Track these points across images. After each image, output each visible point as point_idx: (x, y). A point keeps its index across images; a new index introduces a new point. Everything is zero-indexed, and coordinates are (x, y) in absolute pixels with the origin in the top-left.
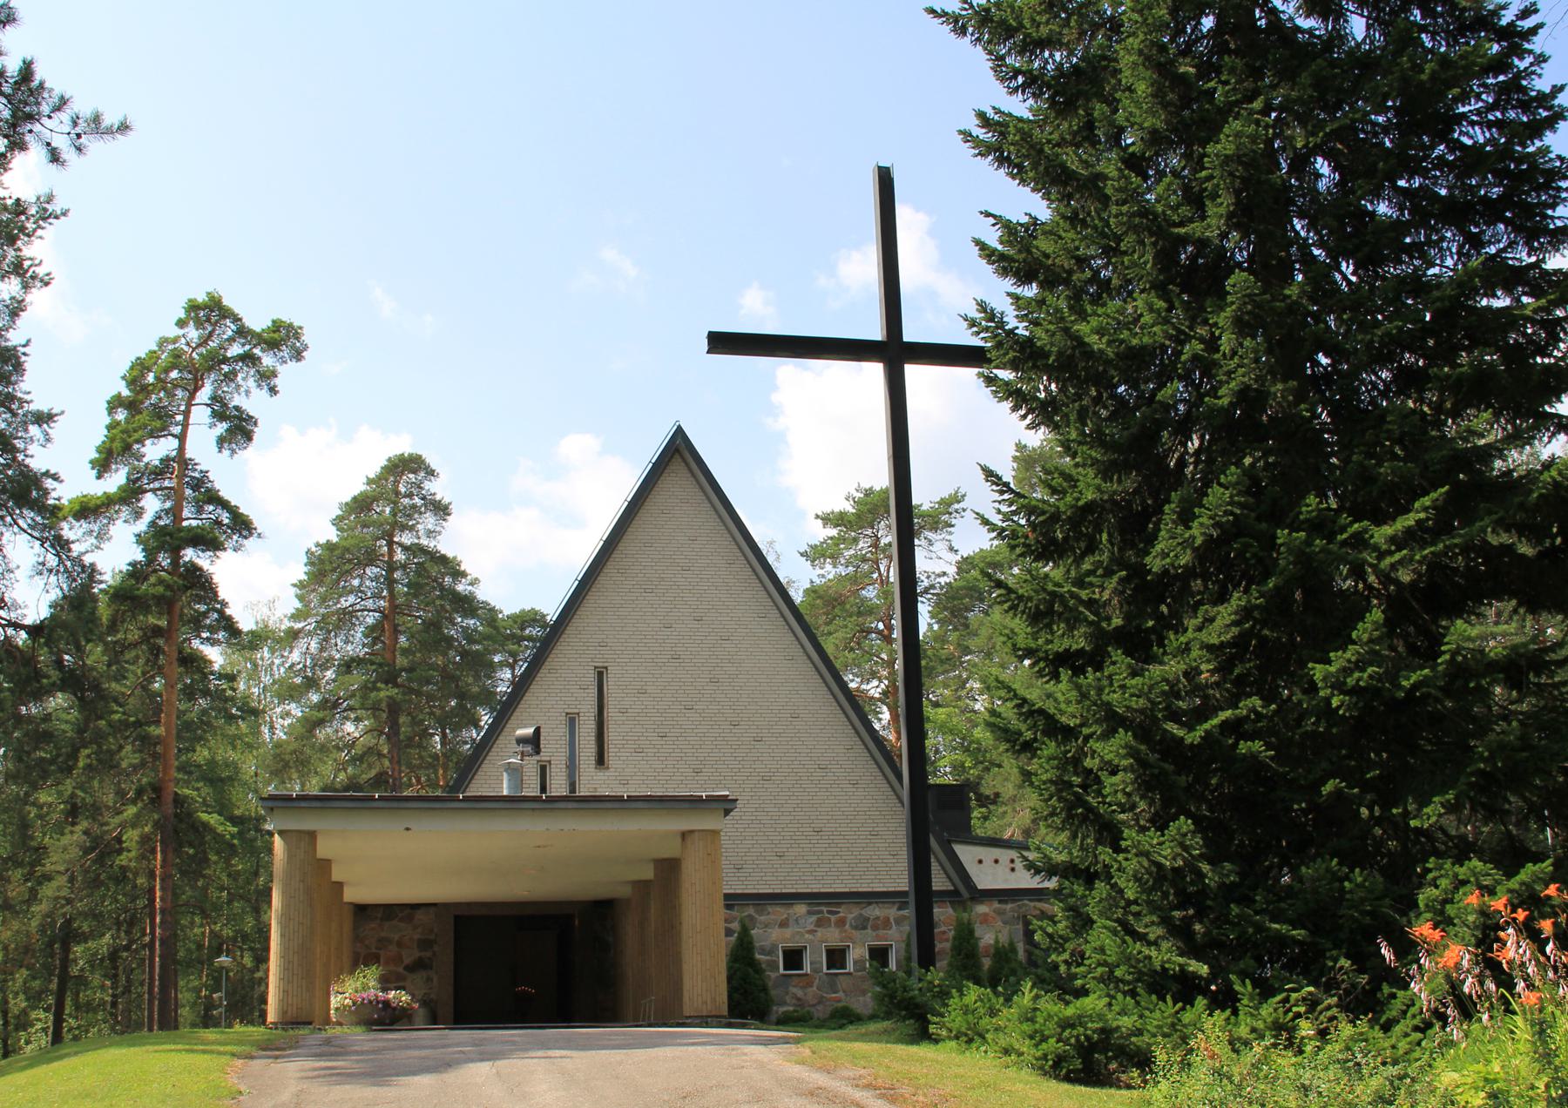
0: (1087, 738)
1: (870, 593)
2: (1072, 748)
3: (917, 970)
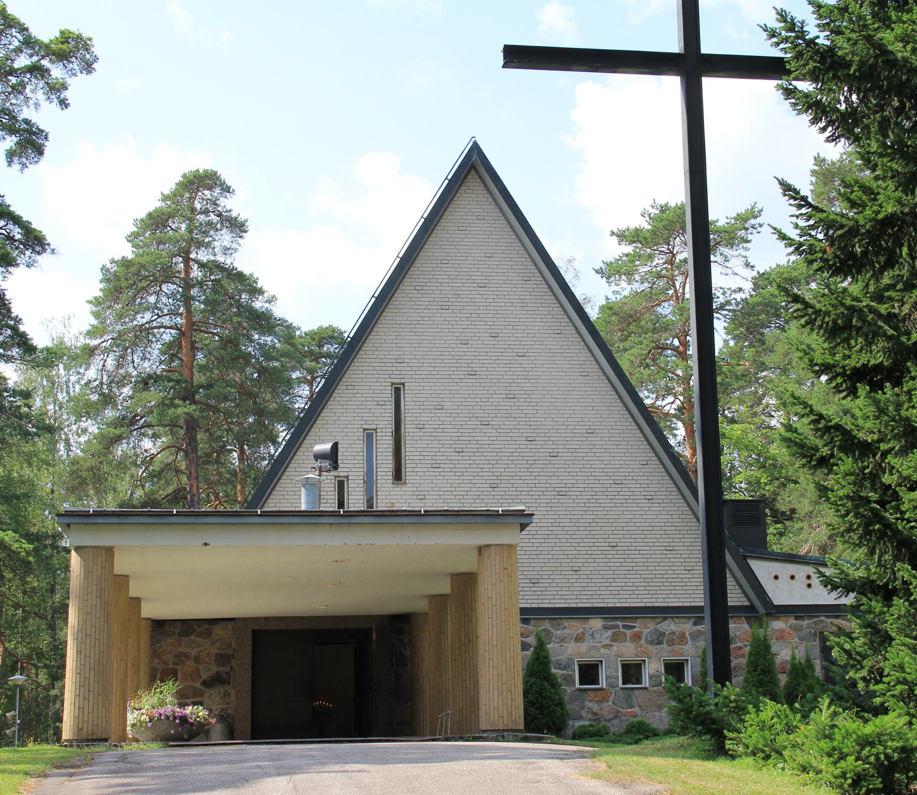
0: (885, 454)
1: (666, 309)
2: (870, 463)
3: (714, 686)
